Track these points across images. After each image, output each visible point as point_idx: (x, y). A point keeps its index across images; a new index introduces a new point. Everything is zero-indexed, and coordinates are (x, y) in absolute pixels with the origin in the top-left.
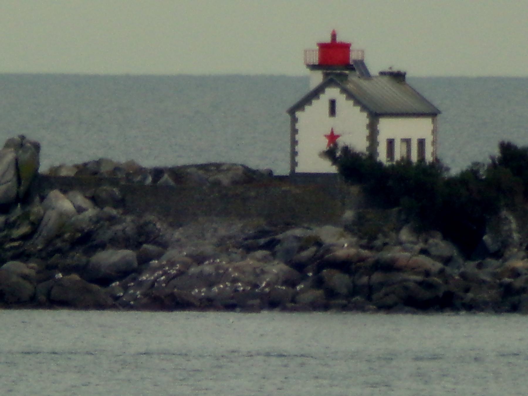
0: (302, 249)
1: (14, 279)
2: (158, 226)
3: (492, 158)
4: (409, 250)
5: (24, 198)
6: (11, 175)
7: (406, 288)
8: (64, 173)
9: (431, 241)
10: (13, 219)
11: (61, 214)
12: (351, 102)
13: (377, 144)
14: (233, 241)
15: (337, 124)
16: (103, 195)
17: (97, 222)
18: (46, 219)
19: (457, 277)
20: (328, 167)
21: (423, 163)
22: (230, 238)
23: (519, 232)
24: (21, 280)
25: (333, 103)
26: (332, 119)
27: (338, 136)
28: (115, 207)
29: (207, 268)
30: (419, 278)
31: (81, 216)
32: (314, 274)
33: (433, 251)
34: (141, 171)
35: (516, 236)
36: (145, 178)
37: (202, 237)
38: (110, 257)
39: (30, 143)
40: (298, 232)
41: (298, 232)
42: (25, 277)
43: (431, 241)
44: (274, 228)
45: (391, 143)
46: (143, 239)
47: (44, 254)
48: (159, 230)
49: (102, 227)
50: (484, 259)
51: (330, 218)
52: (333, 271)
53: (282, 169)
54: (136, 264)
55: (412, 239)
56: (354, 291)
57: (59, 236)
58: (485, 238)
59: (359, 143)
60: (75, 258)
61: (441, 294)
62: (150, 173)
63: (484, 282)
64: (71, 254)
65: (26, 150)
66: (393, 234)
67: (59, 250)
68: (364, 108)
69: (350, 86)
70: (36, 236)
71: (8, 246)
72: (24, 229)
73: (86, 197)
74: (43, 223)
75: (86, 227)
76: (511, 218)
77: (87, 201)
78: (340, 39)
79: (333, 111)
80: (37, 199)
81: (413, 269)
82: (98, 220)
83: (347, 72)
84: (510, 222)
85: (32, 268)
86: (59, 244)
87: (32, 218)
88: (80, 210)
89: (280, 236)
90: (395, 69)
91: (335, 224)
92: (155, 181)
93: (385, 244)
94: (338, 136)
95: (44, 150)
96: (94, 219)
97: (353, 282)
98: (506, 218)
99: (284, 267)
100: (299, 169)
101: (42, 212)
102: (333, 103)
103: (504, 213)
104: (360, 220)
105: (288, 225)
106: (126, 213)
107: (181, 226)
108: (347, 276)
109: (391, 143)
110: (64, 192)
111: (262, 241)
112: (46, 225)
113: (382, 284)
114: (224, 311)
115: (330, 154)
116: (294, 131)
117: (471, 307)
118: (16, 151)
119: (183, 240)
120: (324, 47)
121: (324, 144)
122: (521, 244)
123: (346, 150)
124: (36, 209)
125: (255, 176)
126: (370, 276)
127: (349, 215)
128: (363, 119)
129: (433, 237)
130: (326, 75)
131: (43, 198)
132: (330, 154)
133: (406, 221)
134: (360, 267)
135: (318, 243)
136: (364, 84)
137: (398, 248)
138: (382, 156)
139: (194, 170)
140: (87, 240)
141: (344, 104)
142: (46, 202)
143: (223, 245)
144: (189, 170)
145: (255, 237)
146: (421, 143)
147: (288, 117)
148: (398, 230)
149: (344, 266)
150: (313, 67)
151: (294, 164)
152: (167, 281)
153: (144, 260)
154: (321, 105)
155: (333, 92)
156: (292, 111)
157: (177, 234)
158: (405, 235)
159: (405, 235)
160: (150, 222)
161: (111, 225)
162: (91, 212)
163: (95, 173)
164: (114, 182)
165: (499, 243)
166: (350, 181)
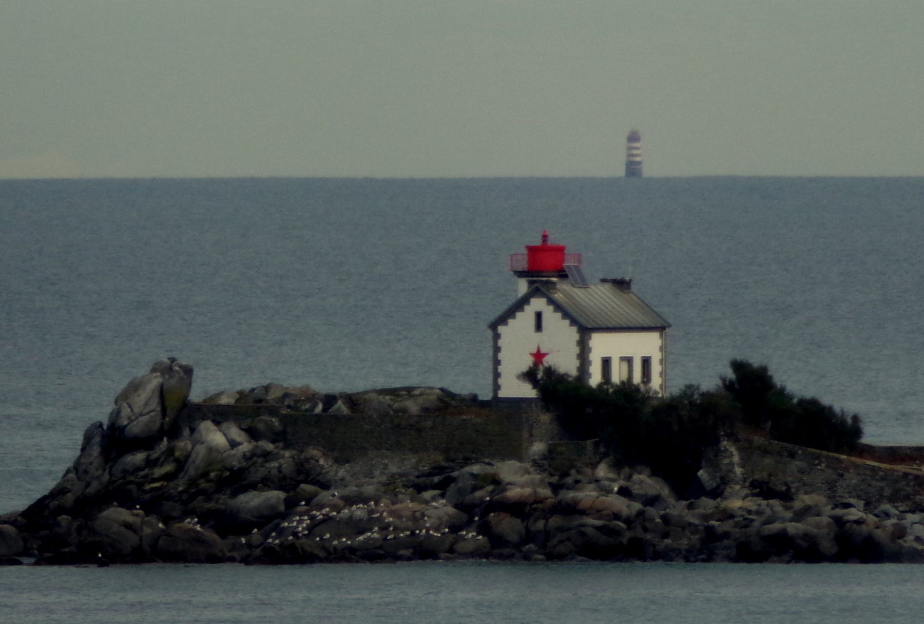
0: (475, 489)
1: (115, 528)
2: (322, 462)
3: (724, 380)
4: (604, 489)
5: (172, 431)
6: (155, 404)
7: (583, 534)
8: (224, 400)
9: (636, 477)
10: (154, 456)
11: (211, 450)
12: (559, 315)
13: (590, 363)
14: (404, 479)
15: (544, 341)
16: (261, 426)
17: (251, 458)
18: (193, 456)
19: (658, 520)
20: (527, 391)
21: (553, 378)
22: (401, 475)
23: (743, 466)
24: (123, 529)
25: (539, 316)
26: (539, 334)
27: (544, 355)
28: (273, 442)
29: (359, 511)
30: (598, 523)
31: (233, 452)
32: (480, 519)
33: (636, 490)
34: (313, 398)
35: (738, 470)
36: (315, 405)
37: (370, 475)
38: (252, 501)
39: (180, 366)
40: (476, 469)
41: (476, 469)
42: (128, 526)
43: (636, 477)
44: (451, 464)
45: (606, 362)
46: (301, 478)
47: (185, 497)
48: (322, 467)
49: (255, 463)
50: (698, 497)
51: (514, 452)
52: (502, 515)
53: (485, 395)
54: (282, 508)
55: (611, 475)
56: (529, 536)
57: (205, 475)
58: (701, 473)
59: (564, 361)
60: (221, 501)
61: (625, 541)
62: (321, 400)
63: (690, 524)
64: (216, 496)
65: (176, 374)
66: (588, 471)
67: (203, 492)
68: (574, 322)
69: (558, 296)
70: (182, 475)
71: (148, 487)
72: (168, 468)
73: (242, 429)
74: (191, 459)
75: (236, 464)
76: (733, 449)
77: (243, 433)
78: (553, 240)
79: (539, 327)
80: (186, 432)
81: (598, 511)
82: (249, 457)
83: (554, 279)
84: (732, 455)
85: (137, 515)
86: (203, 484)
87: (177, 454)
88: (233, 444)
89: (455, 474)
90: (619, 277)
91: (520, 459)
92: (325, 410)
93: (577, 482)
94: (544, 355)
95: (198, 374)
96: (248, 455)
97: (527, 528)
98: (726, 450)
99: (451, 510)
100: (502, 394)
101: (190, 446)
102: (539, 316)
103: (725, 443)
104: (550, 454)
105: (467, 461)
106: (285, 448)
107: (348, 461)
108: (518, 521)
109: (606, 362)
110: (217, 423)
111: (436, 479)
112: (194, 462)
113: (560, 529)
114: (208, 565)
115: (530, 376)
116: (497, 349)
117: (665, 556)
118: (163, 375)
119: (348, 478)
120: (532, 251)
121: (526, 362)
122: (745, 481)
123: (549, 371)
124: (184, 444)
125: (453, 403)
126: (547, 520)
127: (538, 447)
128: (573, 334)
129: (640, 473)
130: (531, 283)
131: (192, 430)
132: (530, 376)
133: (605, 455)
134: (535, 510)
135: (496, 481)
136: (579, 294)
137: (593, 486)
138: (595, 378)
139: (374, 396)
140: (237, 479)
141: (551, 318)
142: (196, 435)
143: (390, 487)
144: (367, 397)
145: (430, 475)
146: (646, 362)
147: (490, 333)
148: (594, 466)
149: (518, 508)
150: (521, 274)
151: (497, 387)
152: (311, 528)
153: (291, 504)
154: (525, 318)
155: (538, 304)
156: (494, 326)
157: (342, 473)
158: (602, 471)
159: (602, 471)
160: (312, 458)
161: (267, 461)
162: (246, 446)
163: (260, 401)
164: (273, 411)
165: (718, 480)
166: (850, 421)
